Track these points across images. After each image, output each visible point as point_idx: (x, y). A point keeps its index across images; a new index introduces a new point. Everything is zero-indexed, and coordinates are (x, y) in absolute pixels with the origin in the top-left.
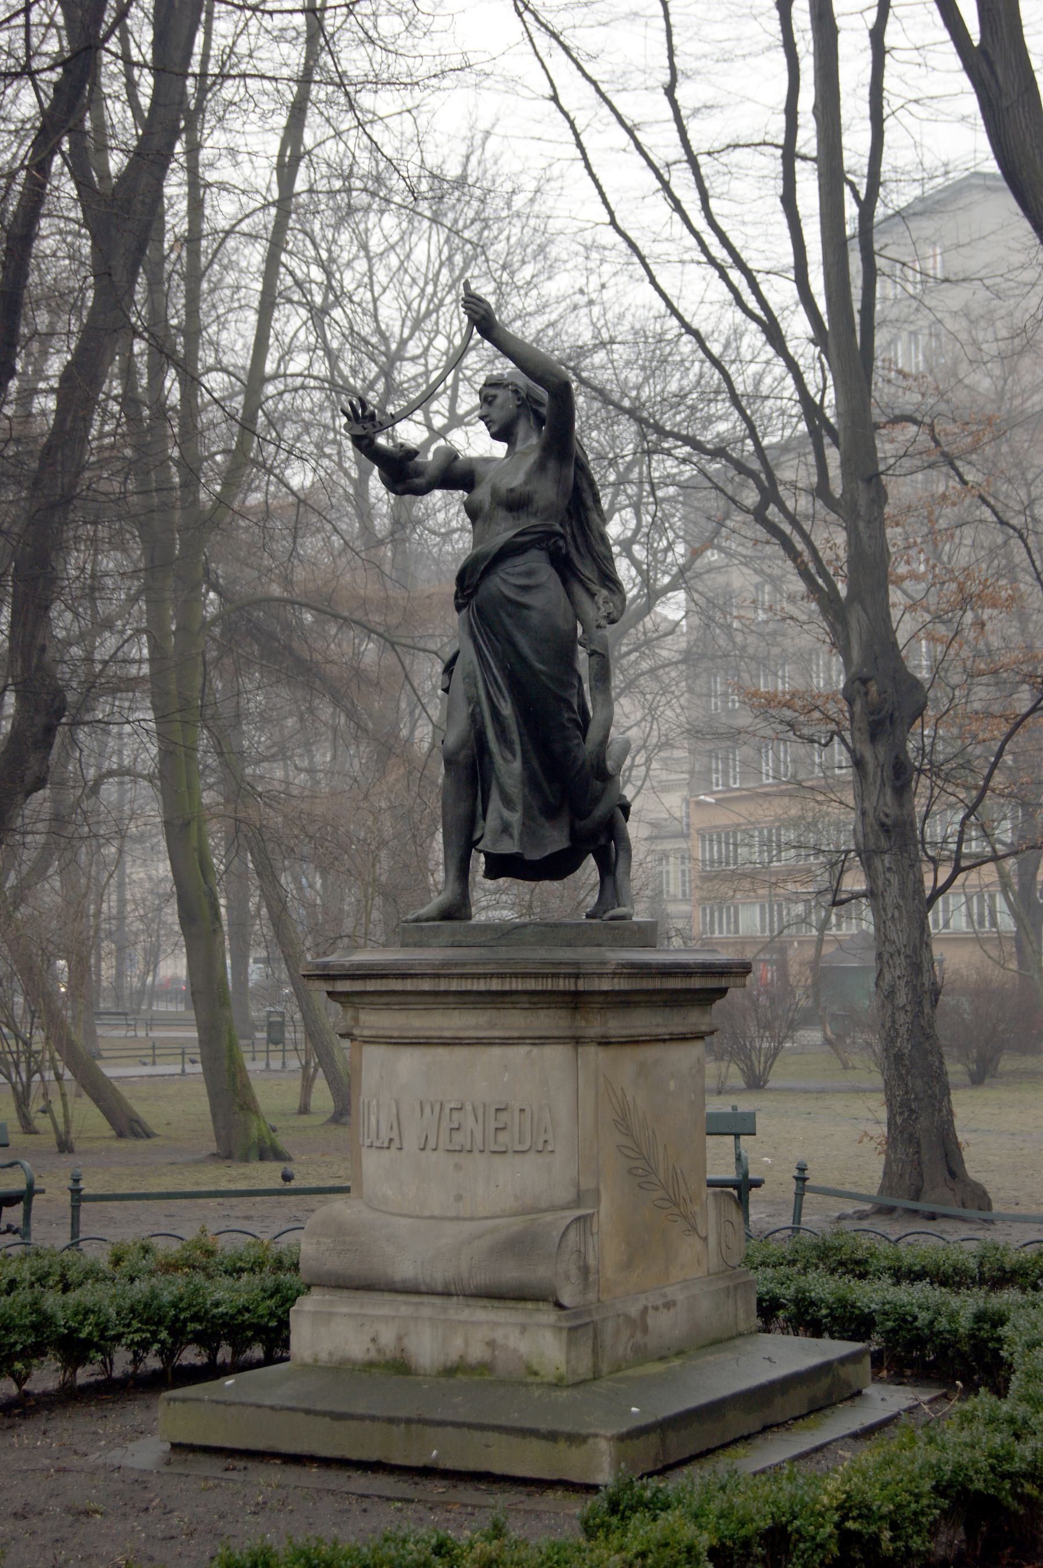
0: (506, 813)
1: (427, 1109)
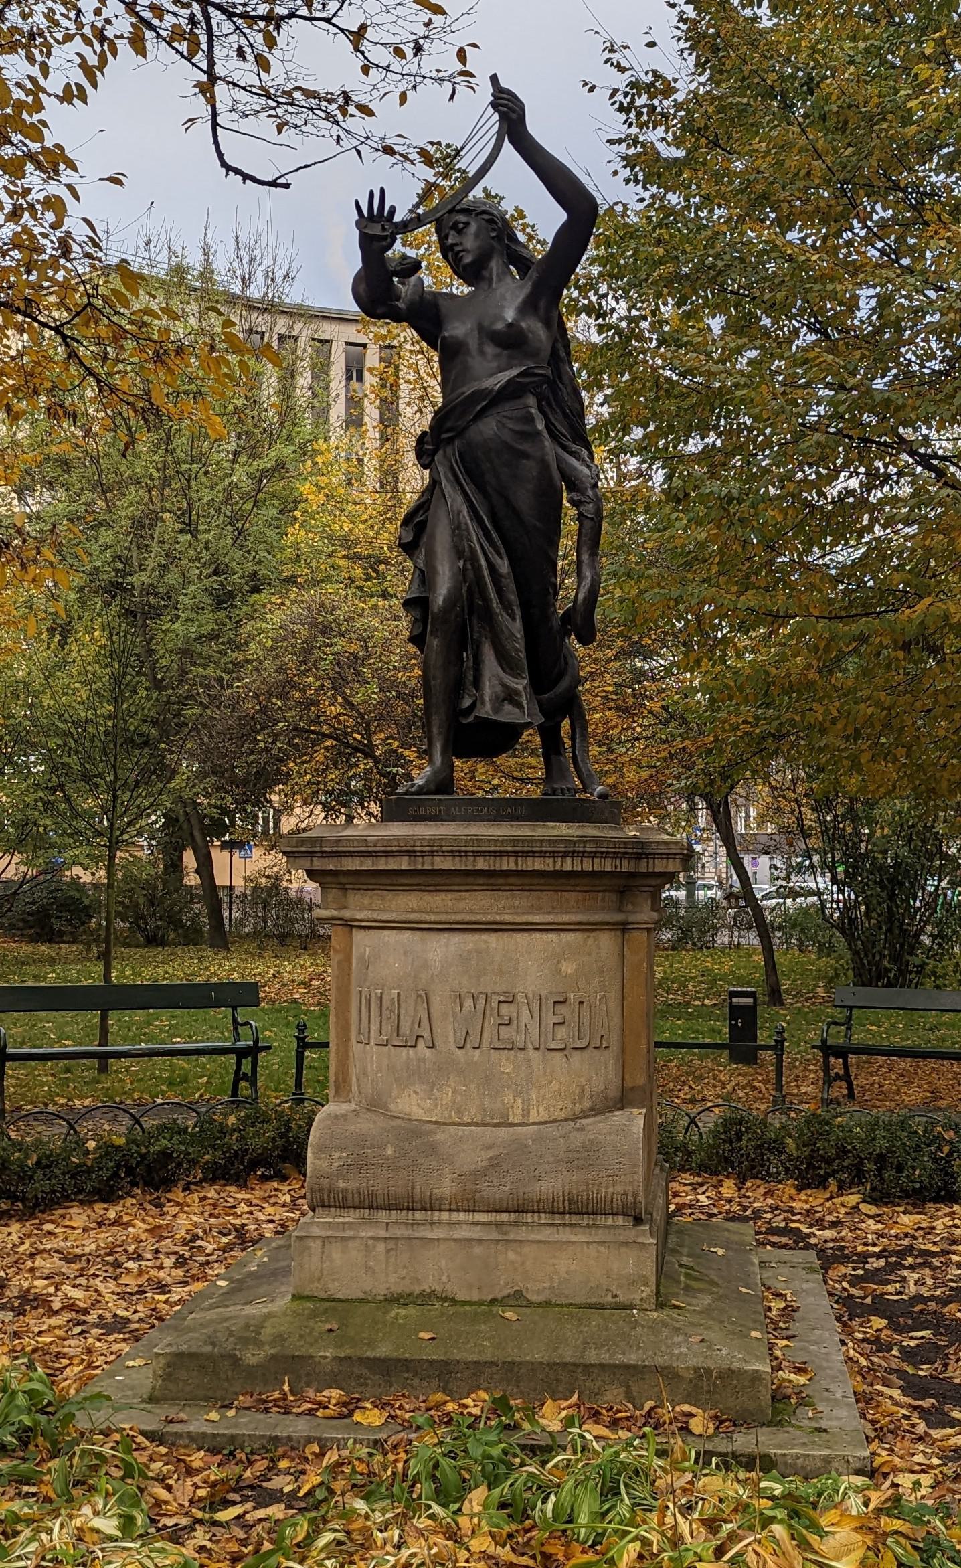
0: (509, 681)
1: (468, 1003)
